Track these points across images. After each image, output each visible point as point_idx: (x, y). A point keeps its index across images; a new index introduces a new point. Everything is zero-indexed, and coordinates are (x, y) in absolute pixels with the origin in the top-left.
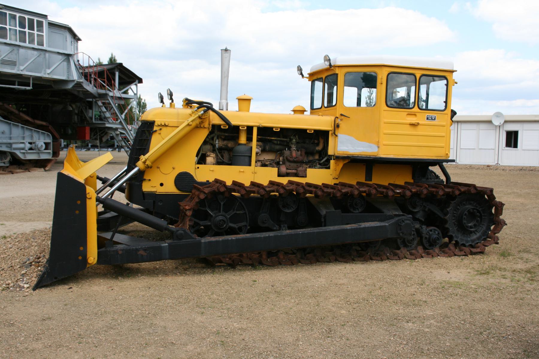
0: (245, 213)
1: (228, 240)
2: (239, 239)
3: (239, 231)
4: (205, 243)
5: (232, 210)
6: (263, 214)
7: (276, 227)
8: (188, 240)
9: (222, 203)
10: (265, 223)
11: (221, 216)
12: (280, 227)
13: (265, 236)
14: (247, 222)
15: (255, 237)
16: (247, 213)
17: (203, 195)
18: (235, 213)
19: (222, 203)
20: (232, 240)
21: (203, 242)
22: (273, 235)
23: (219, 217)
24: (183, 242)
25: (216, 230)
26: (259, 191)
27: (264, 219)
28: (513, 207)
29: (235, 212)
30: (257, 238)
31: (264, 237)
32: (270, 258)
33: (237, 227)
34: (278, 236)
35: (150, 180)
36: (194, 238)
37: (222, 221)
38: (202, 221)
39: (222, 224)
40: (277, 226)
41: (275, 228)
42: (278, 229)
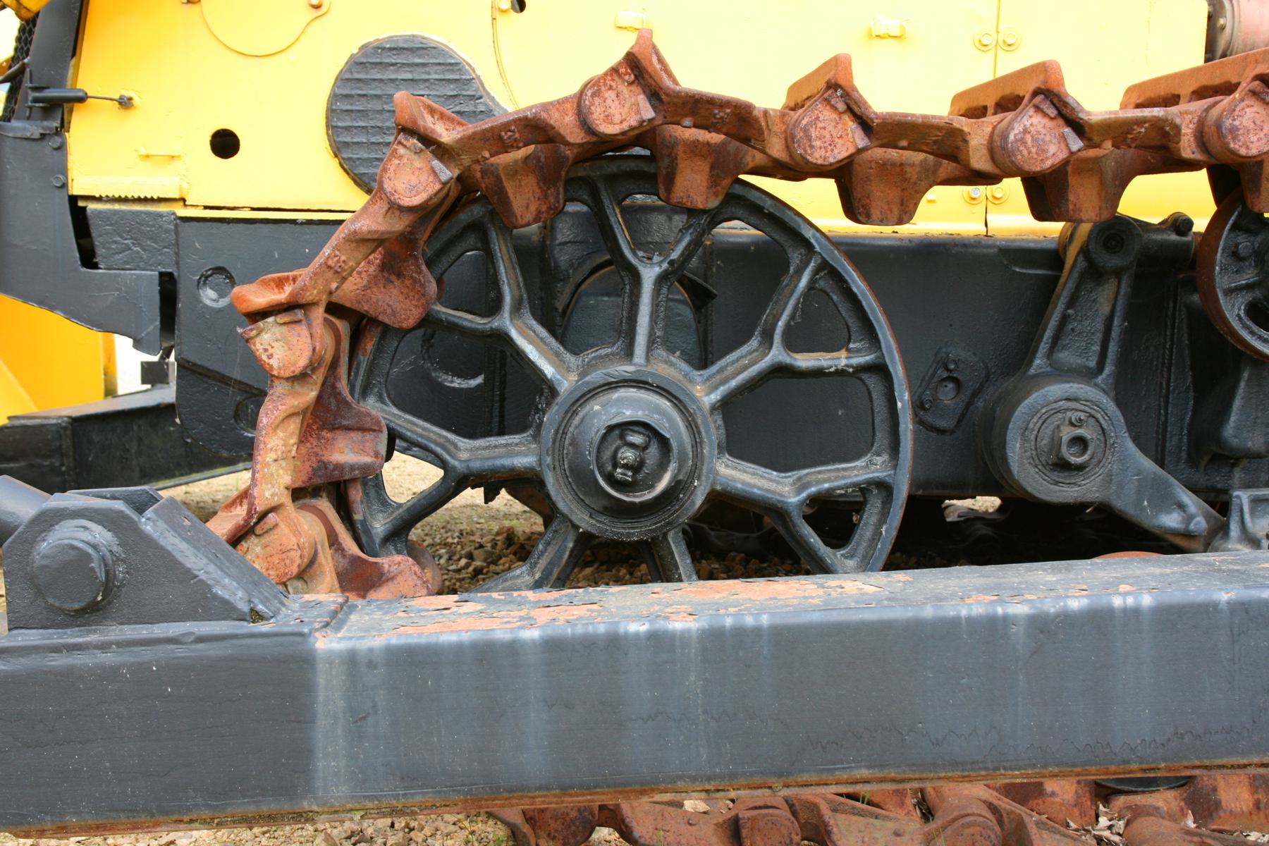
0: (880, 370)
1: (614, 644)
2: (740, 633)
3: (814, 539)
4: (351, 661)
5: (754, 342)
6: (1056, 390)
7: (1181, 507)
8: (159, 630)
9: (649, 274)
10: (1080, 468)
11: (632, 392)
12: (1221, 505)
13: (1051, 607)
14: (894, 449)
15: (928, 612)
16: (898, 371)
17: (418, 163)
18: (781, 371)
19: (649, 274)
20: (659, 641)
21: (331, 657)
22: (1147, 600)
23: (616, 395)
24: (104, 647)
25: (585, 521)
26: (1005, 137)
27: (1067, 433)
28: (253, 549)
29: (777, 354)
30: (954, 624)
31: (1041, 625)
32: (1121, 801)
33: (794, 499)
34: (1208, 610)
35: (125, 103)
36: (227, 611)
37: (637, 439)
38: (471, 434)
39: (636, 468)
40: (1188, 498)
41: (1171, 520)
42: (1200, 524)
